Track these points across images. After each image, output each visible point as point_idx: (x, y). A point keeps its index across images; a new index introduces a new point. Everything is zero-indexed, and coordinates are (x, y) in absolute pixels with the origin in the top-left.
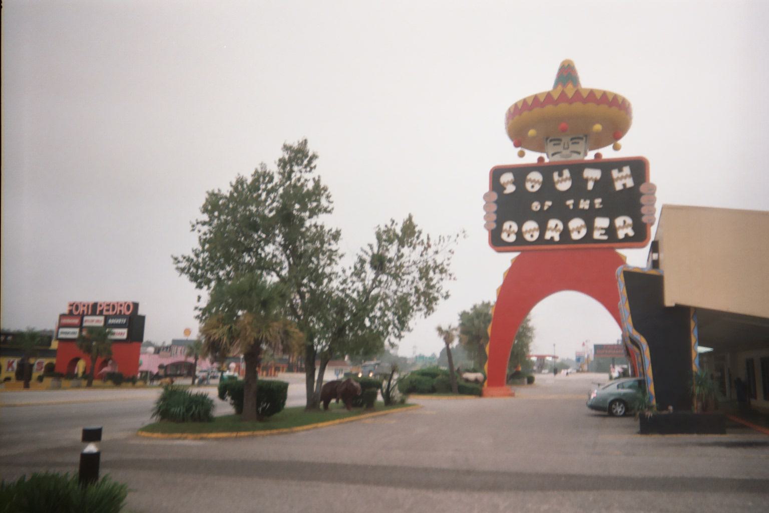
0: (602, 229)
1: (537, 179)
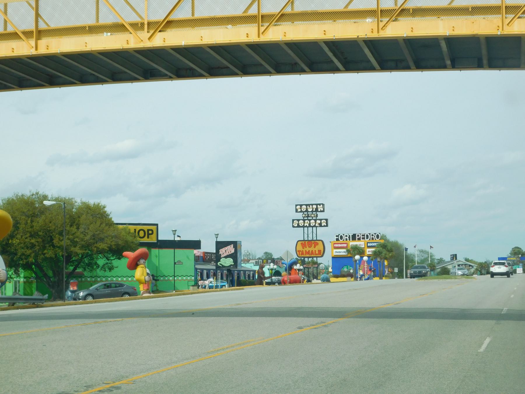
0: (318, 223)
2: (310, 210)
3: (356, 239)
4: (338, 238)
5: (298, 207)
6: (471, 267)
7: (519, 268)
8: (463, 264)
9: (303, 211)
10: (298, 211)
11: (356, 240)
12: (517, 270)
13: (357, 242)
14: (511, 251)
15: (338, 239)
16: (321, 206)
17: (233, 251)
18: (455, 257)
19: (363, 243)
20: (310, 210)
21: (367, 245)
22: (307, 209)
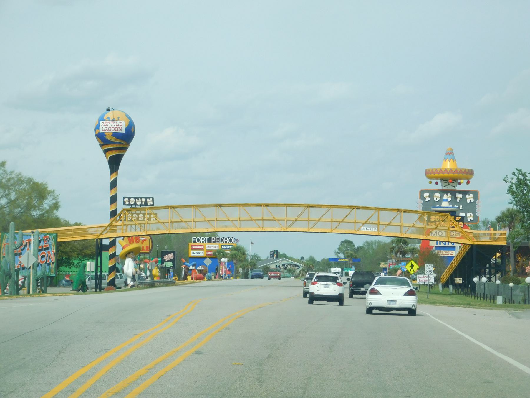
1: (438, 196)
2: (139, 203)
3: (211, 242)
4: (195, 240)
5: (126, 200)
6: (297, 267)
7: (351, 270)
8: (288, 264)
9: (131, 204)
10: (126, 204)
11: (211, 243)
12: (349, 272)
13: (212, 244)
14: (339, 246)
15: (195, 241)
16: (151, 199)
17: (173, 257)
18: (276, 254)
19: (218, 245)
20: (139, 203)
21: (222, 247)
22: (135, 202)
